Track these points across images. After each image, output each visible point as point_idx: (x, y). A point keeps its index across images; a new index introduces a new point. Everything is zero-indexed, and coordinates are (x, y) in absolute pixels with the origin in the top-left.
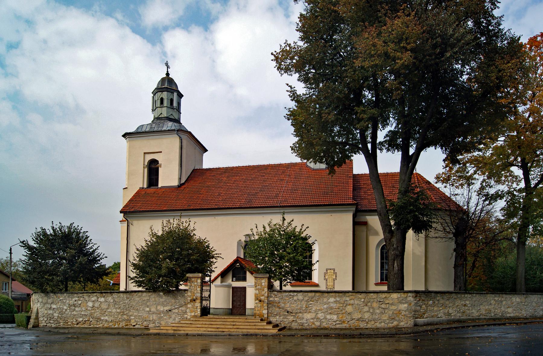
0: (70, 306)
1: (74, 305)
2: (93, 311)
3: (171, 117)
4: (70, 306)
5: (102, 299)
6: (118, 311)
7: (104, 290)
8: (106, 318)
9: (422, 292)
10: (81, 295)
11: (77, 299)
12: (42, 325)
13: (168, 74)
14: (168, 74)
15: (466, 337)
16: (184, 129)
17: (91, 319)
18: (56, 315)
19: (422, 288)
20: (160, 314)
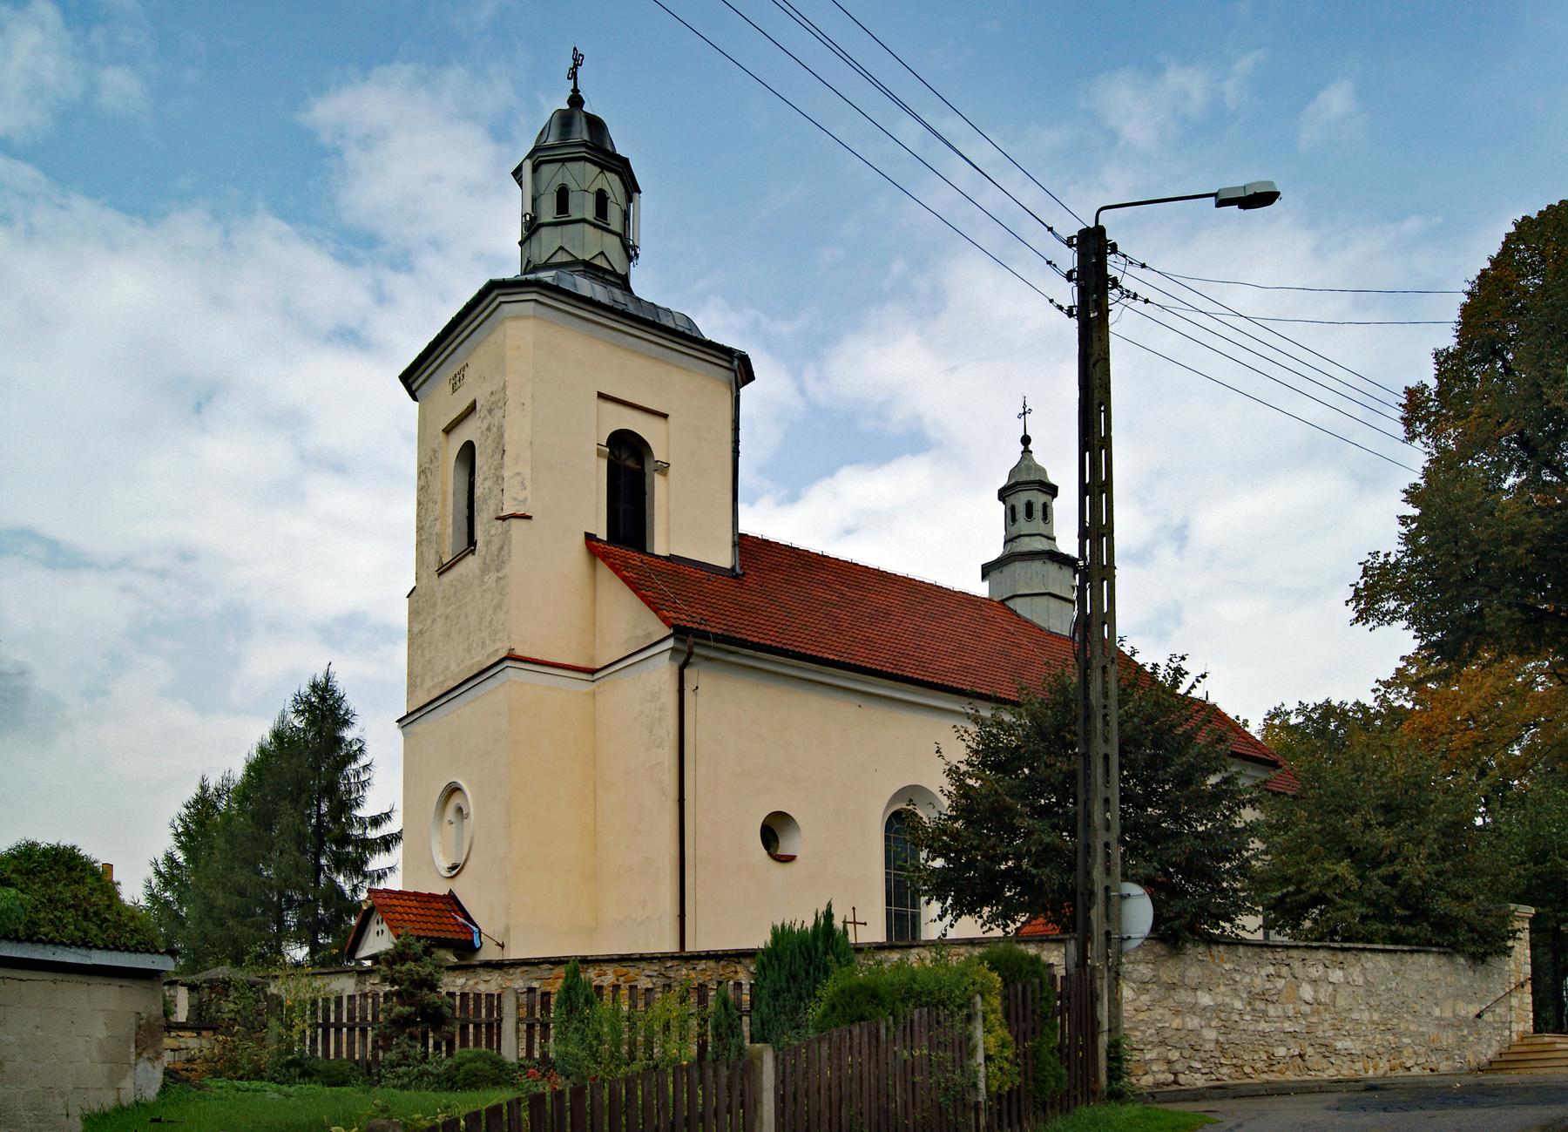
0: (1253, 997)
1: (1263, 996)
2: (1314, 1020)
3: (600, 262)
4: (1253, 997)
5: (1336, 975)
6: (1376, 1017)
7: (1316, 940)
8: (1348, 1043)
9: (672, 957)
10: (1284, 955)
11: (1271, 970)
12: (1148, 1080)
13: (576, 100)
14: (576, 100)
15: (700, 1109)
16: (682, 326)
17: (1310, 1051)
18: (1211, 1034)
19: (670, 946)
20: (1459, 1028)
